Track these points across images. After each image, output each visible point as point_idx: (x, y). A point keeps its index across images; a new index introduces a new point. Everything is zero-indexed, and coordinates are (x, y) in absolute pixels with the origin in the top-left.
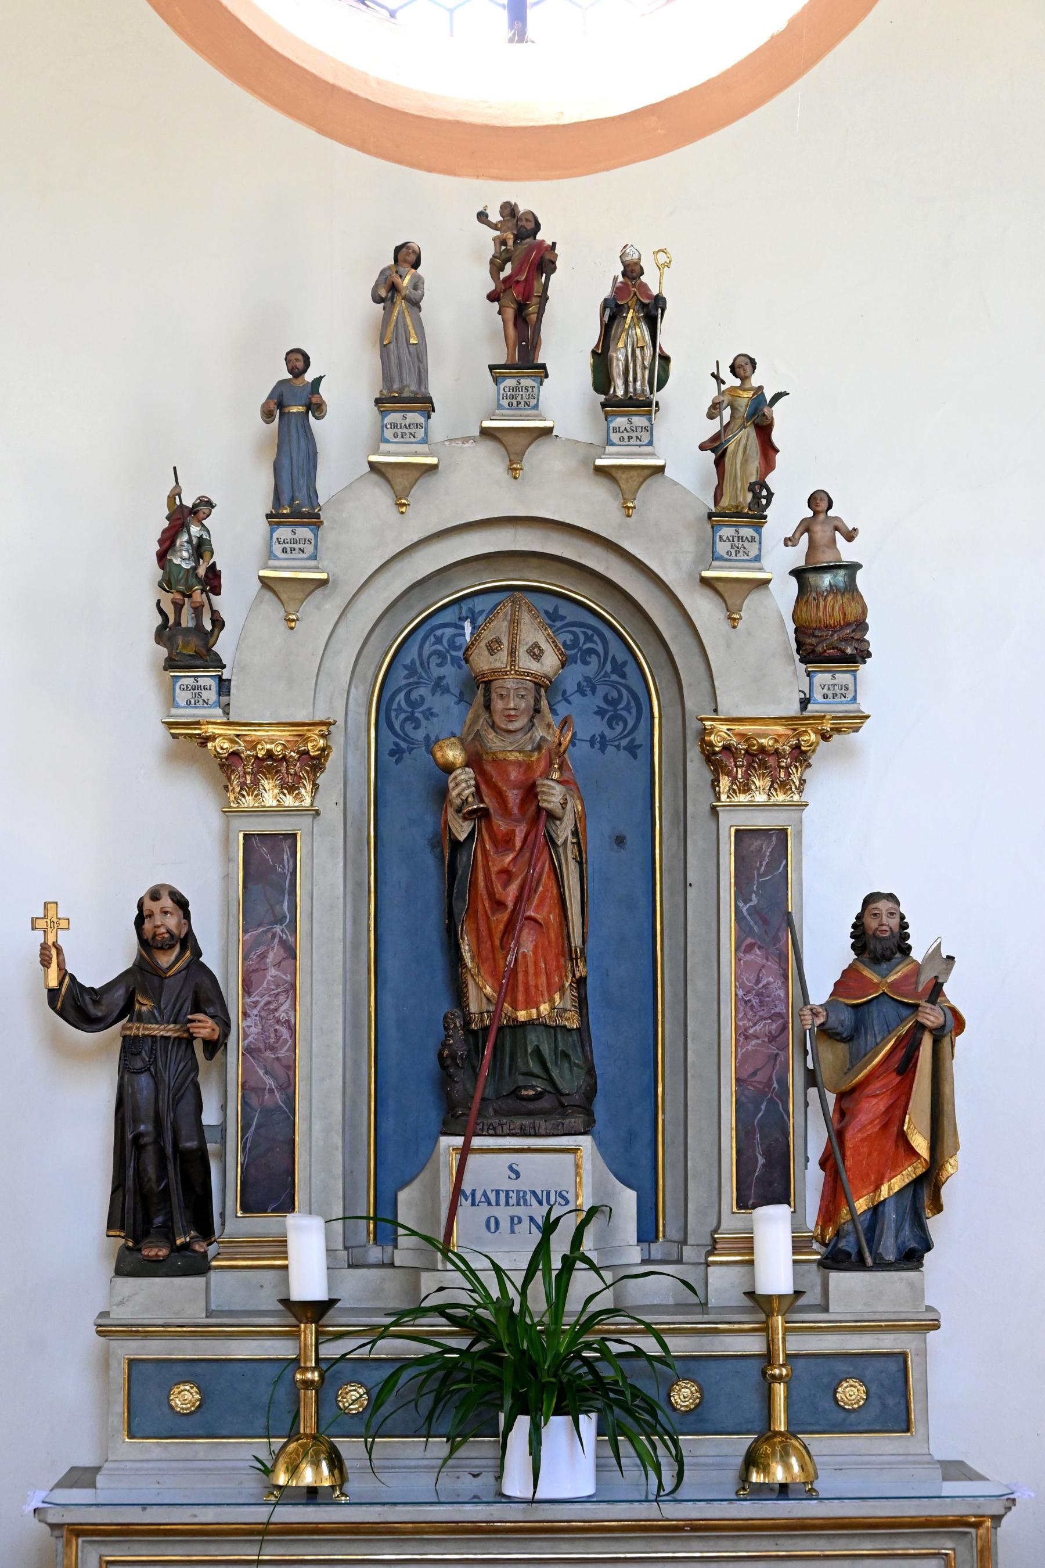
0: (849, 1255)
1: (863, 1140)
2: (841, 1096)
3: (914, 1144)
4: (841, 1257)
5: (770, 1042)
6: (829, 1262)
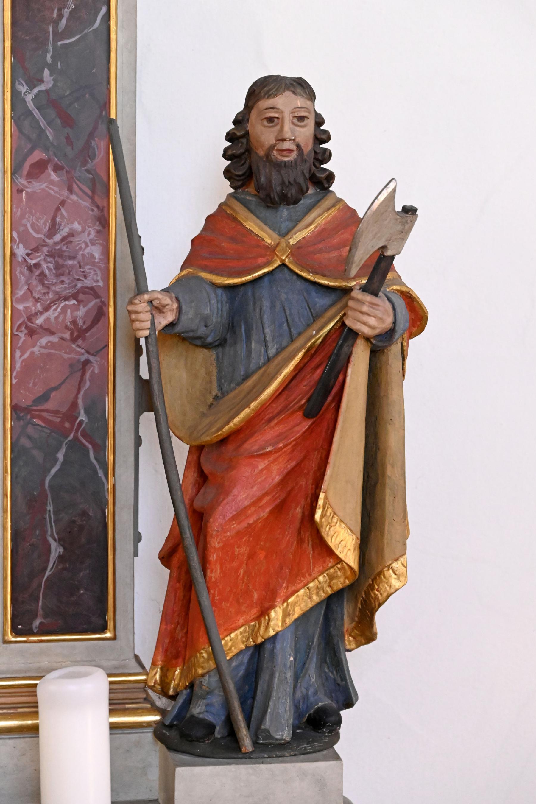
0: (211, 727)
1: (239, 534)
2: (198, 451)
3: (332, 543)
4: (198, 732)
5: (74, 340)
6: (172, 734)
